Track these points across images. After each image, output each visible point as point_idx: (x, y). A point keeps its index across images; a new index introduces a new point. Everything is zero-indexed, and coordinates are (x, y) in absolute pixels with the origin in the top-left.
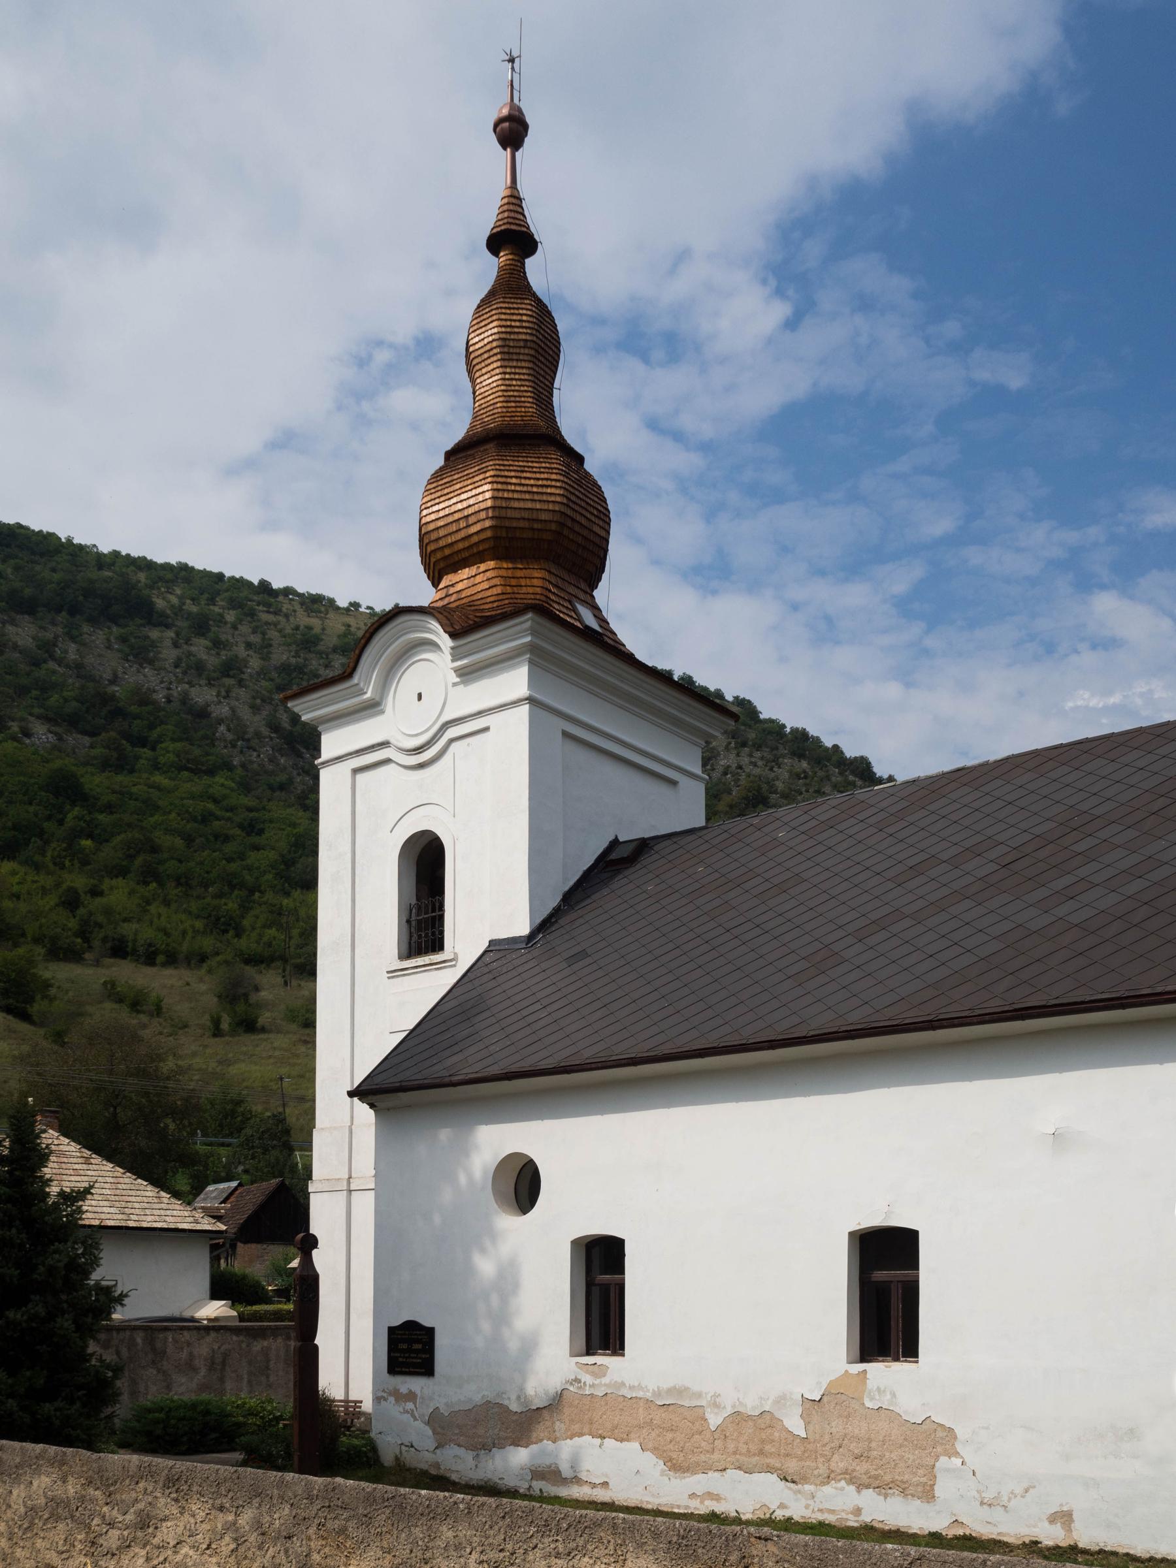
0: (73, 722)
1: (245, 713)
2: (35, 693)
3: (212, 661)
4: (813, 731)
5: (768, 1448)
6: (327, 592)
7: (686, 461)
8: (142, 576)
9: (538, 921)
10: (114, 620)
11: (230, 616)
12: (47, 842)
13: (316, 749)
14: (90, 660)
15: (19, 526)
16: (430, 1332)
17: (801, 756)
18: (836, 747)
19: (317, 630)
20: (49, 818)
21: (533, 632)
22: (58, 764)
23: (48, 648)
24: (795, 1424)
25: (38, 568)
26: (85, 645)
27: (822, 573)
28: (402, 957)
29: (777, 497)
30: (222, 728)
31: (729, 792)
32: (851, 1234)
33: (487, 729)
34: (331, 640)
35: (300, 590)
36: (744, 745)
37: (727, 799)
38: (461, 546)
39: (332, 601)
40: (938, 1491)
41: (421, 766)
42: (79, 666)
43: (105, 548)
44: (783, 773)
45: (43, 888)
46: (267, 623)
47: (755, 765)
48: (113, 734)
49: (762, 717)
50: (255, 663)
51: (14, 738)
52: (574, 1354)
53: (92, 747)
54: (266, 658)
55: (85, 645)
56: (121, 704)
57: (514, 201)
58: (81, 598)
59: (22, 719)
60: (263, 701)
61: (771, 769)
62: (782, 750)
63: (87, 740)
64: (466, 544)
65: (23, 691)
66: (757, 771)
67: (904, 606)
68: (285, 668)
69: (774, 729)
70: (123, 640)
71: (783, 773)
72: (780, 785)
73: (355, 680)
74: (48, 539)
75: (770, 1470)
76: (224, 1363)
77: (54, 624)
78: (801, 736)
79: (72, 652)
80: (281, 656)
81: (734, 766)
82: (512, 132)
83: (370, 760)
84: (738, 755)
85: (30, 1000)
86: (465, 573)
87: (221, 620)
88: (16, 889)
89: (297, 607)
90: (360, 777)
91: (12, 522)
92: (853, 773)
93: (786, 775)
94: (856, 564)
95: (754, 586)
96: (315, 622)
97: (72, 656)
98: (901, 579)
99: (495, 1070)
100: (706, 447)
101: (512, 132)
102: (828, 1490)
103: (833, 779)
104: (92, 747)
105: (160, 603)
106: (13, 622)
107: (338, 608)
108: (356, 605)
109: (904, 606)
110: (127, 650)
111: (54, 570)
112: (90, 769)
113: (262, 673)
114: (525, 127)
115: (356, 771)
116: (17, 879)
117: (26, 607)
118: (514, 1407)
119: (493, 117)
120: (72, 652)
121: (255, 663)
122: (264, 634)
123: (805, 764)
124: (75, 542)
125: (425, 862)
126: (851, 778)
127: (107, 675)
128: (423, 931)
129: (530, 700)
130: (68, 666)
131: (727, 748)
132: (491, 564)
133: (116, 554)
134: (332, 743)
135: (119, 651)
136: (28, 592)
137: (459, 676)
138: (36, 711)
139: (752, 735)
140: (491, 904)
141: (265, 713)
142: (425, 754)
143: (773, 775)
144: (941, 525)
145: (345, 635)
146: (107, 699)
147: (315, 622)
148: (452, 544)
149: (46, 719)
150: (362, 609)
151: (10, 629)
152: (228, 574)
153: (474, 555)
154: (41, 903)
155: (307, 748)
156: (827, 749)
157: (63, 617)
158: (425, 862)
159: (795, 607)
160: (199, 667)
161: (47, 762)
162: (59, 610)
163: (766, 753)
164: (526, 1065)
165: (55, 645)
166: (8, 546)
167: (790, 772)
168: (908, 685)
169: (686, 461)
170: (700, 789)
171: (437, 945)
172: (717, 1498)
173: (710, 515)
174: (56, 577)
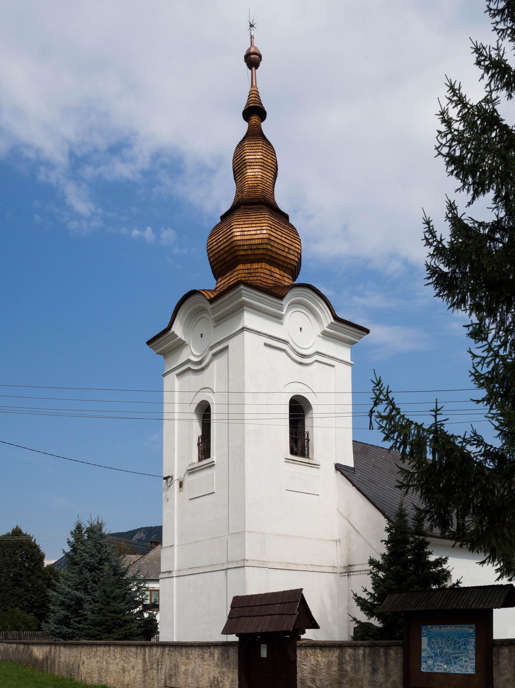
33: (333, 366)
38: (282, 258)
41: (301, 363)
57: (254, 94)
64: (284, 259)
82: (253, 60)
101: (253, 60)
137: (322, 333)
148: (278, 254)
153: (283, 266)
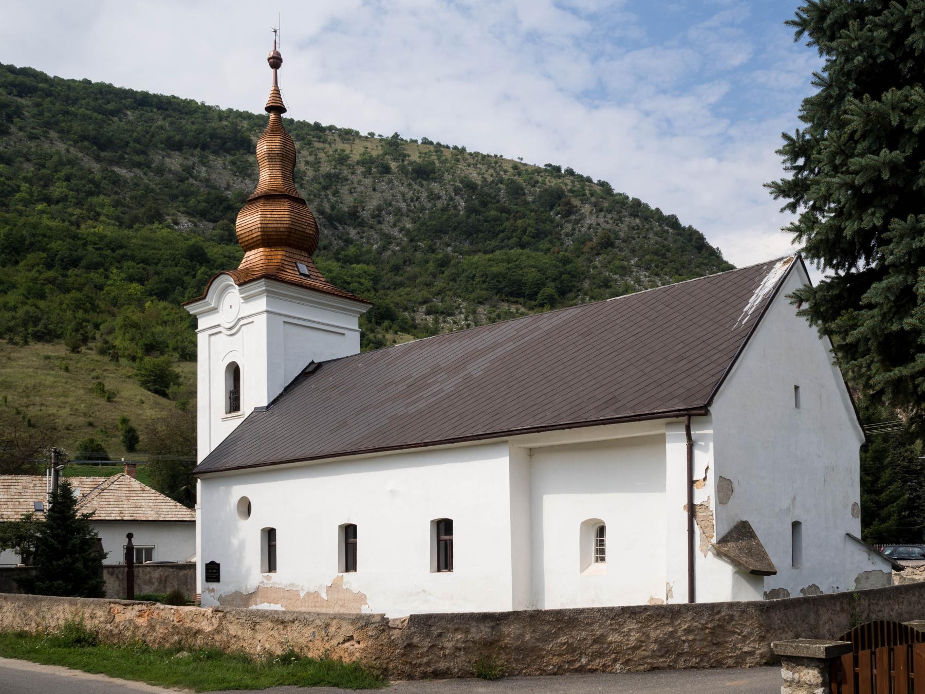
0: (203, 215)
2: (181, 198)
4: (644, 200)
6: (354, 128)
7: (580, 27)
9: (272, 400)
10: (228, 151)
12: (185, 288)
13: (196, 327)
14: (214, 176)
15: (174, 97)
16: (219, 565)
17: (636, 216)
18: (657, 209)
19: (347, 152)
20: (187, 274)
21: (266, 285)
22: (191, 242)
23: (189, 170)
24: (324, 596)
25: (184, 122)
26: (210, 167)
27: (664, 92)
28: (227, 413)
29: (637, 45)
31: (591, 240)
34: (356, 157)
35: (339, 127)
36: (601, 210)
37: (589, 244)
39: (357, 133)
41: (232, 335)
42: (207, 180)
43: (224, 108)
44: (624, 227)
45: (181, 317)
46: (318, 149)
47: (608, 223)
48: (226, 221)
49: (615, 192)
50: (310, 173)
51: (169, 227)
52: (262, 572)
53: (214, 229)
54: (316, 170)
55: (210, 167)
56: (231, 203)
57: (277, 92)
58: (208, 139)
59: (173, 215)
60: (315, 196)
61: (617, 225)
62: (625, 213)
63: (211, 225)
65: (174, 198)
66: (608, 227)
67: (715, 110)
68: (328, 176)
69: (622, 200)
70: (233, 163)
71: (624, 227)
72: (622, 235)
73: (207, 299)
74: (189, 103)
76: (166, 581)
77: (192, 155)
78: (637, 203)
79: (203, 172)
80: (326, 168)
82: (276, 62)
83: (215, 330)
84: (597, 217)
85: (167, 387)
86: (253, 252)
88: (165, 318)
89: (336, 137)
90: (212, 337)
91: (169, 95)
92: (667, 225)
93: (626, 228)
94: (684, 86)
95: (621, 103)
96: (347, 147)
97: (203, 174)
98: (715, 93)
99: (234, 465)
100: (592, 17)
101: (276, 62)
103: (655, 229)
104: (214, 229)
106: (169, 156)
107: (361, 137)
108: (372, 134)
109: (715, 110)
110: (235, 169)
111: (193, 123)
112: (212, 243)
113: (315, 179)
114: (281, 60)
115: (210, 335)
116: (166, 312)
117: (175, 146)
118: (244, 593)
119: (268, 56)
120: (203, 172)
122: (316, 155)
123: (638, 221)
124: (206, 104)
125: (234, 372)
126: (666, 228)
127: (224, 185)
128: (234, 403)
129: (267, 312)
130: (200, 181)
131: (591, 213)
132: (262, 249)
133: (230, 110)
134: (202, 323)
135: (231, 170)
136: (177, 138)
138: (182, 209)
139: (606, 204)
140: (255, 395)
141: (315, 204)
142: (233, 330)
143: (618, 228)
144: (739, 59)
145: (364, 154)
146: (222, 200)
149: (188, 214)
150: (376, 137)
151: (167, 160)
152: (296, 120)
154: (179, 326)
155: (340, 224)
156: (652, 211)
157: (197, 151)
158: (234, 372)
159: (647, 114)
161: (187, 240)
162: (196, 147)
163: (615, 216)
164: (243, 464)
165: (193, 168)
166: (167, 110)
167: (628, 226)
168: (720, 160)
169: (580, 27)
170: (358, 335)
173: (594, 59)
174: (194, 127)
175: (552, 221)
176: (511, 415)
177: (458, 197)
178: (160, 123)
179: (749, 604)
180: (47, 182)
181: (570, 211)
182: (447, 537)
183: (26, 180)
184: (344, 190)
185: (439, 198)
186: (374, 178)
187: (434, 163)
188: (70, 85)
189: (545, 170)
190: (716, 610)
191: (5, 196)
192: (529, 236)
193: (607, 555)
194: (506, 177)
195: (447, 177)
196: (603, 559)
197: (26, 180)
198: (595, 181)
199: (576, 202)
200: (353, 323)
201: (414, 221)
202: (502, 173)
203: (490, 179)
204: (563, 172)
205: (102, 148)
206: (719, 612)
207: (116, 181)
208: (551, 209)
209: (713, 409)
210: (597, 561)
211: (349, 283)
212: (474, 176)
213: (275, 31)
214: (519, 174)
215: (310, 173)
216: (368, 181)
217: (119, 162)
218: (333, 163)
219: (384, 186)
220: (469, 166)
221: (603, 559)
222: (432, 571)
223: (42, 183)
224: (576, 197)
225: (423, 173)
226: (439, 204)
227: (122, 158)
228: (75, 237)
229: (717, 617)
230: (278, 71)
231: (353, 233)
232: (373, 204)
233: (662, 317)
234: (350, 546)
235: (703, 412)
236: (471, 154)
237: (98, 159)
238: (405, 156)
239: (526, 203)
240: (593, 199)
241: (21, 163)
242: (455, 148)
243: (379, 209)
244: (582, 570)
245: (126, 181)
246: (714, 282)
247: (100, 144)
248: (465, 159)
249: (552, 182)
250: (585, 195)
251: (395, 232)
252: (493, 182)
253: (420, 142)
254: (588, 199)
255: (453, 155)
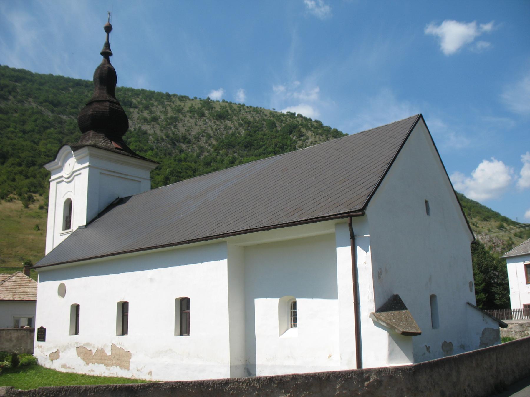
1: (158, 132)
3: (148, 117)
5: (103, 358)
6: (187, 95)
8: (130, 94)
9: (89, 221)
11: (156, 103)
19: (182, 106)
28: (63, 230)
30: (151, 137)
32: (118, 303)
36: (317, 134)
40: (130, 368)
57: (107, 45)
68: (172, 118)
75: (103, 363)
81: (314, 141)
82: (108, 29)
87: (153, 105)
89: (177, 99)
90: (58, 185)
96: (182, 104)
101: (108, 29)
102: (112, 368)
105: (134, 101)
108: (196, 98)
113: (166, 120)
121: (162, 117)
122: (166, 108)
125: (69, 205)
128: (67, 224)
131: (312, 135)
147: (182, 104)
158: (69, 205)
160: (145, 120)
171: (69, 228)
172: (93, 371)
175: (291, 140)
176: (229, 223)
177: (241, 128)
178: (86, 93)
179: (397, 370)
180: (24, 123)
181: (301, 135)
182: (187, 311)
183: (14, 121)
184: (180, 125)
185: (231, 128)
186: (196, 119)
187: (227, 111)
188: (41, 76)
189: (287, 115)
190: (365, 376)
191: (1, 129)
192: (279, 147)
193: (298, 323)
194: (266, 118)
195: (235, 118)
196: (295, 326)
197: (14, 121)
198: (313, 120)
199: (303, 130)
200: (147, 174)
201: (217, 140)
202: (264, 116)
203: (257, 119)
204: (296, 115)
205: (55, 105)
206: (368, 379)
207: (61, 122)
208: (291, 134)
209: (368, 211)
210: (292, 327)
211: (181, 173)
212: (250, 118)
213: (109, 14)
214: (273, 117)
215: (162, 117)
216: (193, 121)
217: (63, 112)
218: (175, 112)
219: (201, 123)
220: (247, 112)
221: (295, 326)
222: (176, 335)
223: (22, 123)
224: (303, 128)
225: (222, 116)
226: (231, 132)
227: (65, 110)
228: (35, 150)
229: (366, 384)
230: (110, 34)
231: (184, 146)
232: (194, 132)
233: (333, 157)
234: (184, 316)
235: (360, 213)
236: (247, 107)
237: (52, 112)
238: (212, 108)
239: (277, 131)
240: (312, 129)
241: (12, 113)
242: (240, 104)
243: (199, 134)
244: (281, 334)
245: (65, 122)
246: (368, 134)
247: (55, 104)
248: (244, 109)
249: (290, 120)
250: (308, 127)
251: (206, 146)
252: (259, 120)
253: (221, 101)
254: (310, 129)
255: (238, 107)
